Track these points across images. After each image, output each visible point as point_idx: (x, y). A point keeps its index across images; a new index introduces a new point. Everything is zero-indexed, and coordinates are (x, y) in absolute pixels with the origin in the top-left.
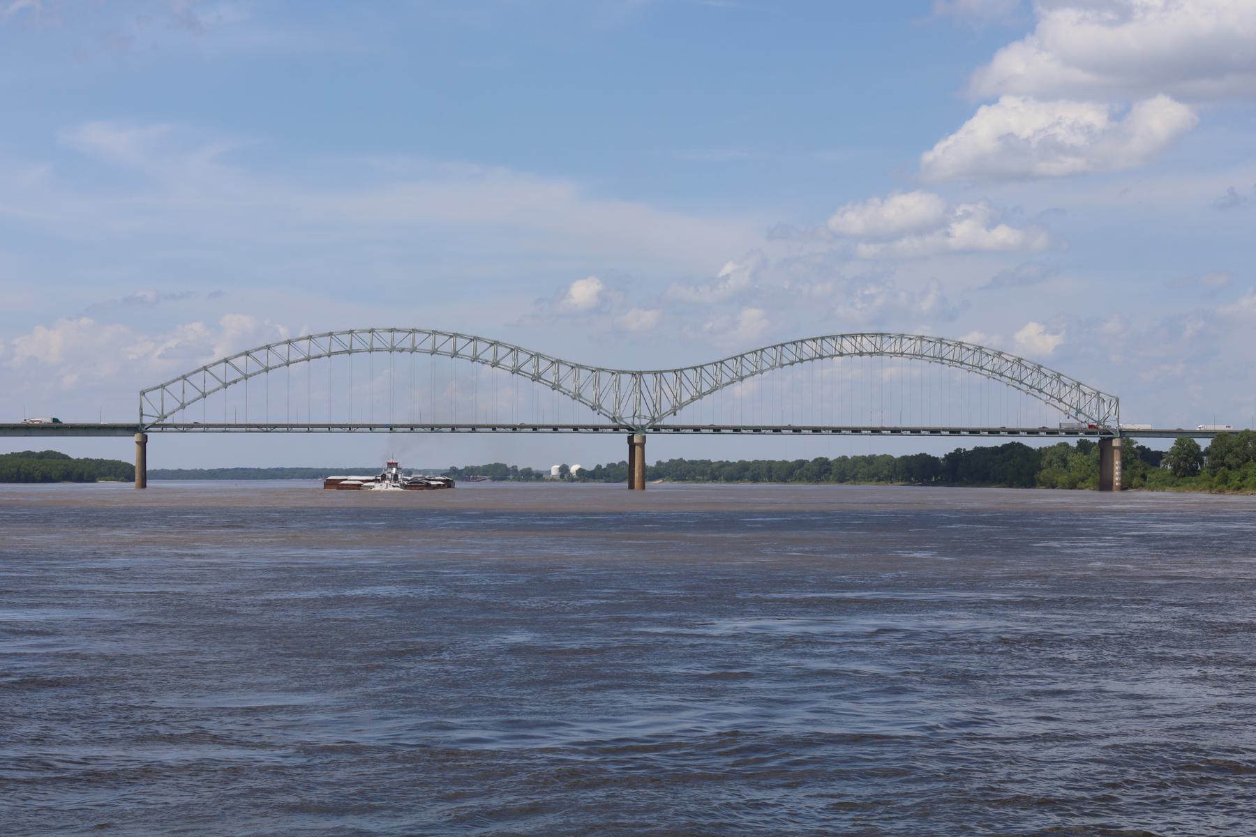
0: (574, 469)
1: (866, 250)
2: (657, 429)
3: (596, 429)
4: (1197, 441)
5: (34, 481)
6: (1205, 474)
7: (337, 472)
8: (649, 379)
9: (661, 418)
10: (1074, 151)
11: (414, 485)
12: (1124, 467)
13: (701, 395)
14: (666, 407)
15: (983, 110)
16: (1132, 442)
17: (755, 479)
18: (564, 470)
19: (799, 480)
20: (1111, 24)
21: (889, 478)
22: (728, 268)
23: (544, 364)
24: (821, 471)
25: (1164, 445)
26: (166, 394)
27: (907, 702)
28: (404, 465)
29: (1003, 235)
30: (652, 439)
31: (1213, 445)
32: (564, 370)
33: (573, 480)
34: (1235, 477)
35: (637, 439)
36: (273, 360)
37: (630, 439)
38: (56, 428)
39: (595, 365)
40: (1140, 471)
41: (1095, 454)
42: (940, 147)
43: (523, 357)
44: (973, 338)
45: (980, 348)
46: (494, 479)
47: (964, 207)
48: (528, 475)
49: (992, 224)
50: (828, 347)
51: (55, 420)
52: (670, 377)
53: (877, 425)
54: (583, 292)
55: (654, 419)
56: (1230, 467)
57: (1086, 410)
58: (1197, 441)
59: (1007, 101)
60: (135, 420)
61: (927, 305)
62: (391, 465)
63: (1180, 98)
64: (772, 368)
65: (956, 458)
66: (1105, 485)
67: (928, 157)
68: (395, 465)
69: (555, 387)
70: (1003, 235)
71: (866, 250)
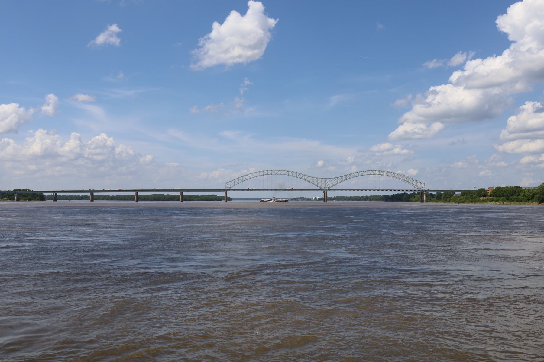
0: (317, 198)
1: (378, 154)
2: (329, 190)
3: (317, 190)
4: (441, 192)
5: (209, 200)
6: (442, 199)
7: (263, 199)
8: (328, 180)
9: (330, 188)
10: (419, 134)
11: (278, 201)
12: (426, 197)
13: (338, 183)
14: (331, 185)
15: (400, 127)
16: (428, 193)
17: (353, 200)
18: (315, 198)
19: (362, 200)
20: (427, 107)
21: (380, 200)
22: (349, 158)
23: (306, 177)
24: (366, 198)
25: (434, 193)
26: (231, 184)
27: (513, 235)
28: (276, 197)
29: (405, 151)
30: (328, 192)
31: (444, 193)
32: (310, 178)
33: (317, 200)
34: (448, 200)
35: (325, 192)
36: (248, 177)
37: (324, 192)
38: (104, 191)
39: (317, 177)
40: (430, 198)
41: (420, 194)
42: (392, 133)
43: (302, 176)
44: (399, 172)
45: (400, 174)
46: (301, 200)
47: (397, 146)
48: (308, 199)
49: (403, 149)
50: (368, 173)
51: (90, 190)
52: (332, 179)
53: (374, 189)
54: (320, 163)
55: (329, 188)
56: (447, 198)
57: (418, 186)
58: (441, 192)
59: (405, 124)
60: (225, 188)
61: (390, 165)
62: (273, 197)
63: (442, 122)
64: (353, 177)
65: (393, 196)
66: (422, 201)
67: (390, 135)
68: (274, 197)
69: (309, 181)
70: (405, 151)
71: (378, 154)
